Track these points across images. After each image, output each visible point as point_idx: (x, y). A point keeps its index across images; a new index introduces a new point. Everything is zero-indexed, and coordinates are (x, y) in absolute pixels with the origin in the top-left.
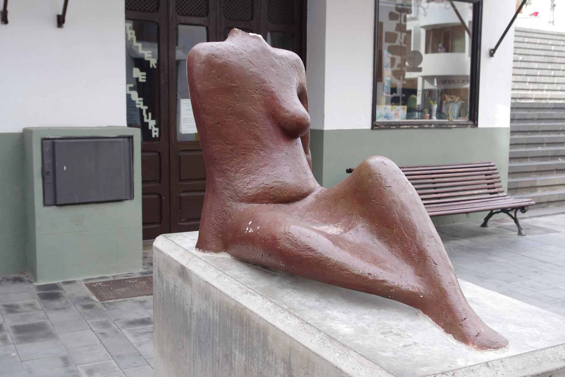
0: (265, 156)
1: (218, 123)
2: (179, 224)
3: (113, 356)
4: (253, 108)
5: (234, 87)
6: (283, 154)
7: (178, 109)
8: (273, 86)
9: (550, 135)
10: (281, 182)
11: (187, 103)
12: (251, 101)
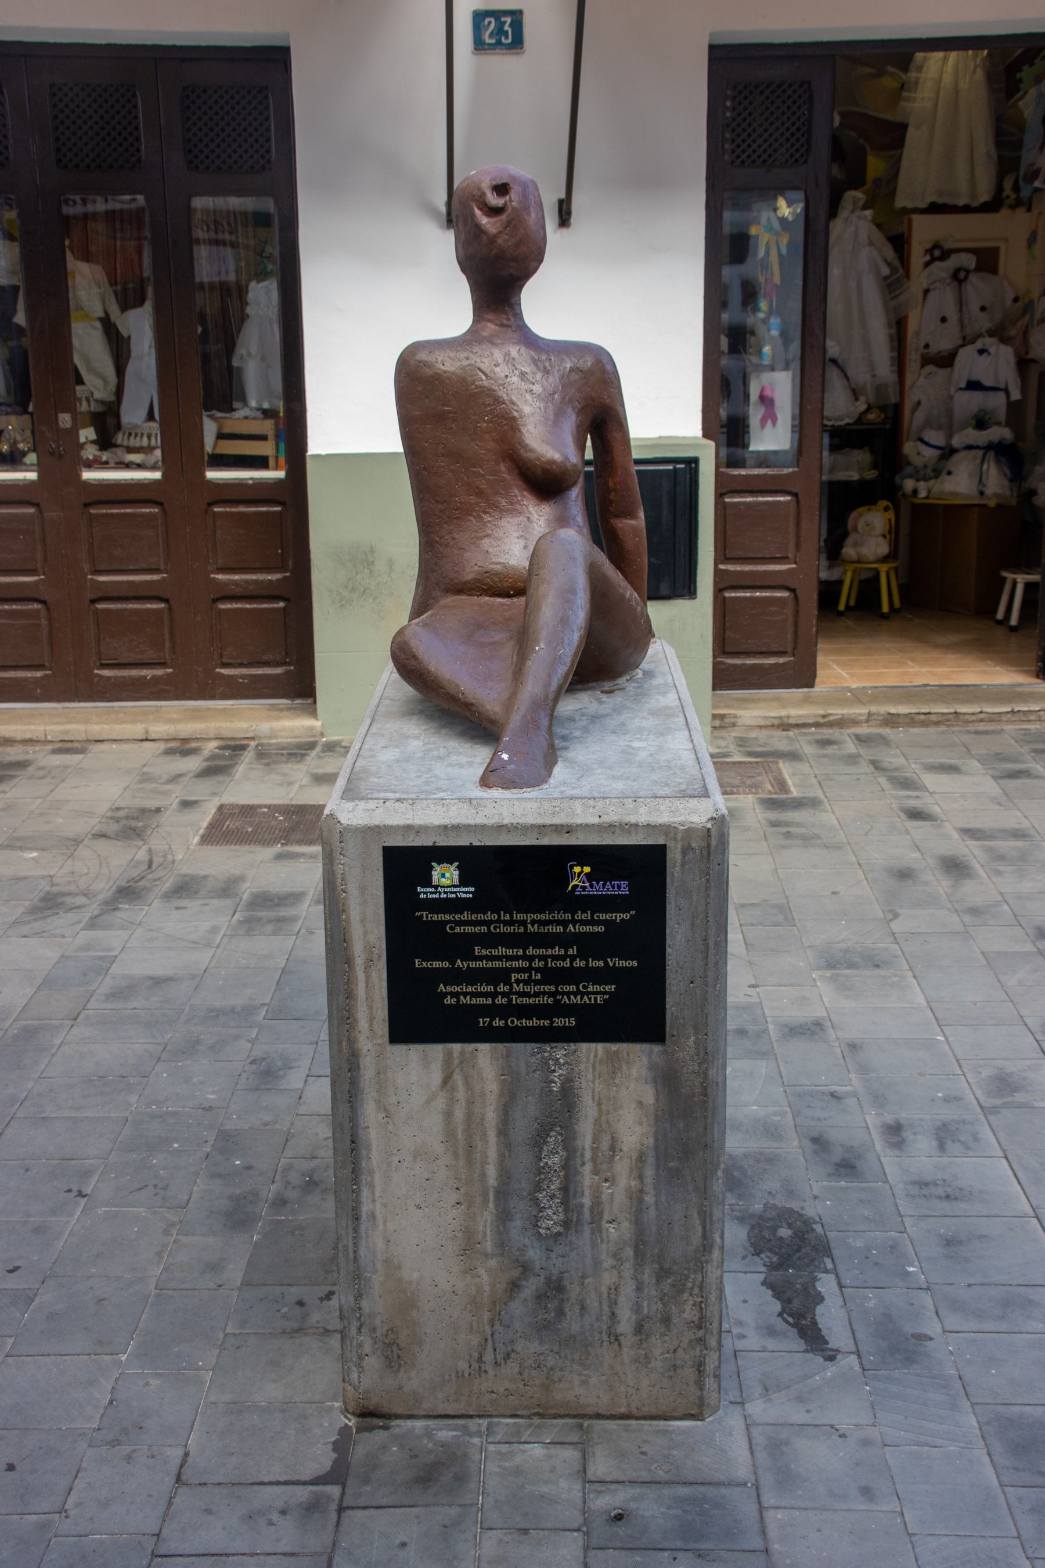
0: (489, 521)
1: (425, 469)
2: (212, 576)
3: (1016, 1534)
4: (477, 445)
5: (449, 412)
6: (521, 518)
7: (224, 468)
8: (515, 408)
9: (757, 497)
10: (503, 564)
11: (277, 458)
12: (476, 433)
